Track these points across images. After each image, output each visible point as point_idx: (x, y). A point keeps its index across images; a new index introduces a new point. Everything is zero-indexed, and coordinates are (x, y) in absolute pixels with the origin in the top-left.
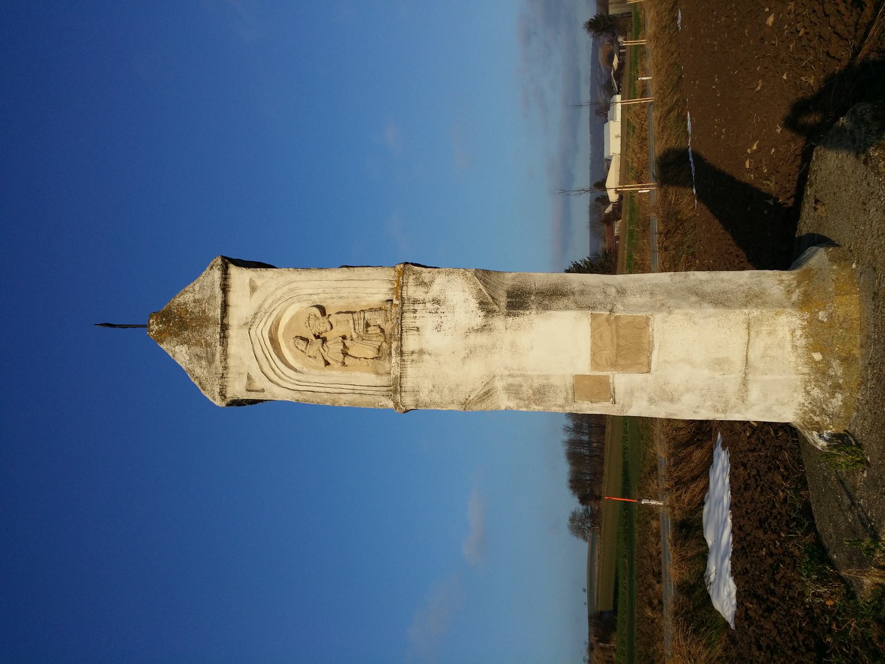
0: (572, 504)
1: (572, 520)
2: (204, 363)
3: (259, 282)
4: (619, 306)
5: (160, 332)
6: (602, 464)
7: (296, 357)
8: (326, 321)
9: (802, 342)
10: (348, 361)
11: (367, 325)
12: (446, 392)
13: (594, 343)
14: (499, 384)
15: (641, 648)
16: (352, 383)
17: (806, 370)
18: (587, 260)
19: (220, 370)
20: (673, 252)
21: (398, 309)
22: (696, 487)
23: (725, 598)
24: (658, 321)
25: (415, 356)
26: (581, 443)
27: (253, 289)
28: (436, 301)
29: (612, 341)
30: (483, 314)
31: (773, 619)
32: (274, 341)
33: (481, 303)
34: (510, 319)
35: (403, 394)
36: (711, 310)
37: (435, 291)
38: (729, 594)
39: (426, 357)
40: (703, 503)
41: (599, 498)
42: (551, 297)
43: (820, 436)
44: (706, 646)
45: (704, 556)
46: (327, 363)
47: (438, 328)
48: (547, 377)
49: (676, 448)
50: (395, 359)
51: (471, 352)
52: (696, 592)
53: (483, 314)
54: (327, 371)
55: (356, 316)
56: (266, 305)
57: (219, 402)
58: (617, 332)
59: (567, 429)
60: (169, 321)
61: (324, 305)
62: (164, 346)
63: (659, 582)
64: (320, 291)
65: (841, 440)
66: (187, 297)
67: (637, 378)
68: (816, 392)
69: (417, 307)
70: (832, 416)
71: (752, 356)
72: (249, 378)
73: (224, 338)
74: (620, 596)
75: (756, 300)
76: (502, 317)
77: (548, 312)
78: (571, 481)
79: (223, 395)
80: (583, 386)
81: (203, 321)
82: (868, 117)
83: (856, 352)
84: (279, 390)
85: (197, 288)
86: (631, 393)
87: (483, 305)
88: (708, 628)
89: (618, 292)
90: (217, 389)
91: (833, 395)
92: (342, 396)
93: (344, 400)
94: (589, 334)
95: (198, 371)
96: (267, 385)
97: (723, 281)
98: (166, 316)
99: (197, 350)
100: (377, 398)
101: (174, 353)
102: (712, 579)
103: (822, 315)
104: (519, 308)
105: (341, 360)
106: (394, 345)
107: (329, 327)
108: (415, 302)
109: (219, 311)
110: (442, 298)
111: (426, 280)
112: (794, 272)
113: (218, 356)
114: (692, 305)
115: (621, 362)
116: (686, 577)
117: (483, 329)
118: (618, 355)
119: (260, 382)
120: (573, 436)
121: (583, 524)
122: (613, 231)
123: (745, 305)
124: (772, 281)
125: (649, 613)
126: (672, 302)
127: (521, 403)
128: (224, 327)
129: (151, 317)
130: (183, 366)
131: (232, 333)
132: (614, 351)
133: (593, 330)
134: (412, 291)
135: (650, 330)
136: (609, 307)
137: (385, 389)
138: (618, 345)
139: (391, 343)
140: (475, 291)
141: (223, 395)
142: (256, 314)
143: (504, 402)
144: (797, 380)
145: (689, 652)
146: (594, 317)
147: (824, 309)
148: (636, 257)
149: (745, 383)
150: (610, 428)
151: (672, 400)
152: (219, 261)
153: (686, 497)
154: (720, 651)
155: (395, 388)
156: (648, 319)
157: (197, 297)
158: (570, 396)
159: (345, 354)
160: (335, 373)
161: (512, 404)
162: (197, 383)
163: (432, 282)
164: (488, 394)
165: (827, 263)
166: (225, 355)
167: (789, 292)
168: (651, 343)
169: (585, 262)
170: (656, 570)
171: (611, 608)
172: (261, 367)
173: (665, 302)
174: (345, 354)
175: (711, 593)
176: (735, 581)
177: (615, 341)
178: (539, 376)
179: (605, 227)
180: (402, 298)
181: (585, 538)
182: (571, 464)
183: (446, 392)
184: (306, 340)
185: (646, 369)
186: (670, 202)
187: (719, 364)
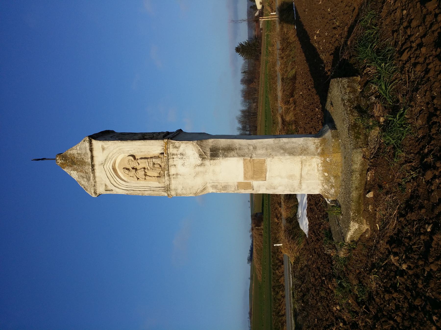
2: (85, 180)
3: (105, 146)
4: (254, 155)
5: (62, 164)
7: (124, 176)
8: (136, 162)
9: (321, 168)
10: (147, 178)
11: (154, 164)
12: (188, 189)
13: (245, 170)
14: (208, 185)
15: (273, 235)
16: (148, 186)
17: (322, 179)
18: (247, 42)
19: (93, 183)
20: (285, 60)
21: (166, 158)
23: (304, 225)
24: (269, 161)
25: (174, 176)
27: (103, 149)
28: (182, 154)
30: (201, 159)
31: (319, 244)
32: (114, 169)
33: (200, 155)
34: (212, 161)
35: (171, 191)
36: (288, 157)
37: (181, 150)
38: (306, 224)
39: (179, 176)
42: (228, 151)
43: (328, 200)
44: (297, 244)
45: (296, 206)
46: (138, 179)
47: (183, 165)
48: (227, 183)
50: (167, 178)
51: (197, 174)
52: (293, 221)
53: (201, 159)
54: (138, 181)
55: (149, 160)
56: (110, 156)
57: (94, 196)
58: (253, 165)
60: (66, 160)
61: (134, 154)
62: (65, 170)
63: (280, 207)
64: (133, 149)
65: (335, 201)
66: (74, 151)
67: (261, 182)
68: (326, 186)
69: (174, 156)
70: (331, 195)
71: (303, 174)
72: (106, 185)
73: (93, 170)
74: (264, 207)
75: (305, 152)
76: (209, 160)
77: (227, 158)
79: (95, 193)
80: (240, 185)
81: (82, 163)
82: (346, 86)
84: (119, 190)
85: (78, 148)
86: (259, 187)
87: (201, 155)
88: (298, 237)
89: (254, 148)
90: (93, 191)
91: (331, 188)
92: (145, 192)
93: (146, 193)
95: (83, 183)
96: (113, 188)
97: (293, 142)
98: (65, 158)
99: (82, 174)
100: (160, 192)
101: (71, 174)
102: (300, 216)
103: (328, 159)
104: (215, 157)
105: (144, 178)
106: (166, 172)
107: (138, 165)
108: (173, 155)
109: (90, 160)
110: (184, 153)
111: (177, 146)
112: (320, 138)
113: (92, 178)
114: (281, 154)
115: (255, 176)
116: (289, 215)
117: (201, 165)
118: (254, 174)
119: (110, 187)
120: (242, 132)
122: (259, 26)
123: (300, 154)
124: (311, 143)
125: (276, 220)
126: (273, 153)
127: (218, 191)
128: (93, 166)
129: (57, 156)
130: (75, 179)
131: (96, 167)
134: (171, 150)
136: (250, 155)
137: (163, 188)
138: (254, 170)
139: (164, 171)
140: (197, 150)
141: (95, 193)
142: (106, 160)
143: (211, 190)
144: (319, 182)
145: (290, 247)
147: (329, 157)
148: (270, 49)
149: (300, 183)
150: (260, 119)
151: (274, 189)
152: (88, 139)
154: (303, 246)
155: (167, 189)
156: (265, 160)
157: (79, 152)
158: (237, 188)
159: (146, 175)
160: (141, 182)
161: (214, 191)
162: (83, 187)
163: (179, 147)
164: (204, 189)
165: (331, 138)
166: (94, 177)
167: (317, 148)
168: (266, 169)
169: (246, 43)
170: (279, 202)
171: (261, 211)
172: (110, 181)
173: (272, 152)
174: (146, 175)
175: (299, 222)
176: (308, 219)
178: (224, 183)
179: (255, 23)
180: (168, 154)
183: (188, 189)
184: (128, 169)
185: (264, 179)
186: (284, 32)
187: (291, 177)
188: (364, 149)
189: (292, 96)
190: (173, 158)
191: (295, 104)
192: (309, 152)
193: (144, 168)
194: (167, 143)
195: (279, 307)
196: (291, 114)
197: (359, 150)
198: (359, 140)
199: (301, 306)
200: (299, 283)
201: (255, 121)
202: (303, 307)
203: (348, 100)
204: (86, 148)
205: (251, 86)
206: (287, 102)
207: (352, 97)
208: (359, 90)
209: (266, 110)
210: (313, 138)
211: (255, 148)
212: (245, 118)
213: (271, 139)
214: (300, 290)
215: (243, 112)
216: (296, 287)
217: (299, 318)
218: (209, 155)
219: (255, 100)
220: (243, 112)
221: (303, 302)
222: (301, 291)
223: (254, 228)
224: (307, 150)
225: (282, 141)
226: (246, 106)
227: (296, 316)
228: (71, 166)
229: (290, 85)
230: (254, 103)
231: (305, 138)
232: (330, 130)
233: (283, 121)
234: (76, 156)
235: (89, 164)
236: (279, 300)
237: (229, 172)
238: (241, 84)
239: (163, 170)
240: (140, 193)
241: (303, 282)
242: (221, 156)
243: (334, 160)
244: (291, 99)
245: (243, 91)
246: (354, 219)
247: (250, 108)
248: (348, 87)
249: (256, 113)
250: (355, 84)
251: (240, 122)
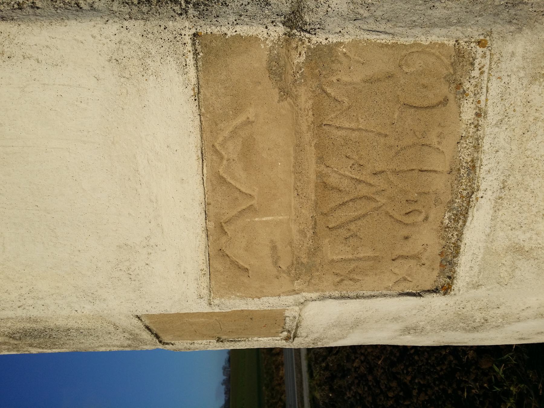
13: (217, 183)
29: (298, 169)
58: (319, 126)
94: (193, 141)
115: (334, 250)
132: (307, 213)
135: (468, 112)
138: (324, 186)
146: (208, 53)
156: (461, 58)
177: (312, 167)
185: (429, 277)
199: (328, 396)
214: (324, 364)
221: (331, 390)
222: (327, 368)
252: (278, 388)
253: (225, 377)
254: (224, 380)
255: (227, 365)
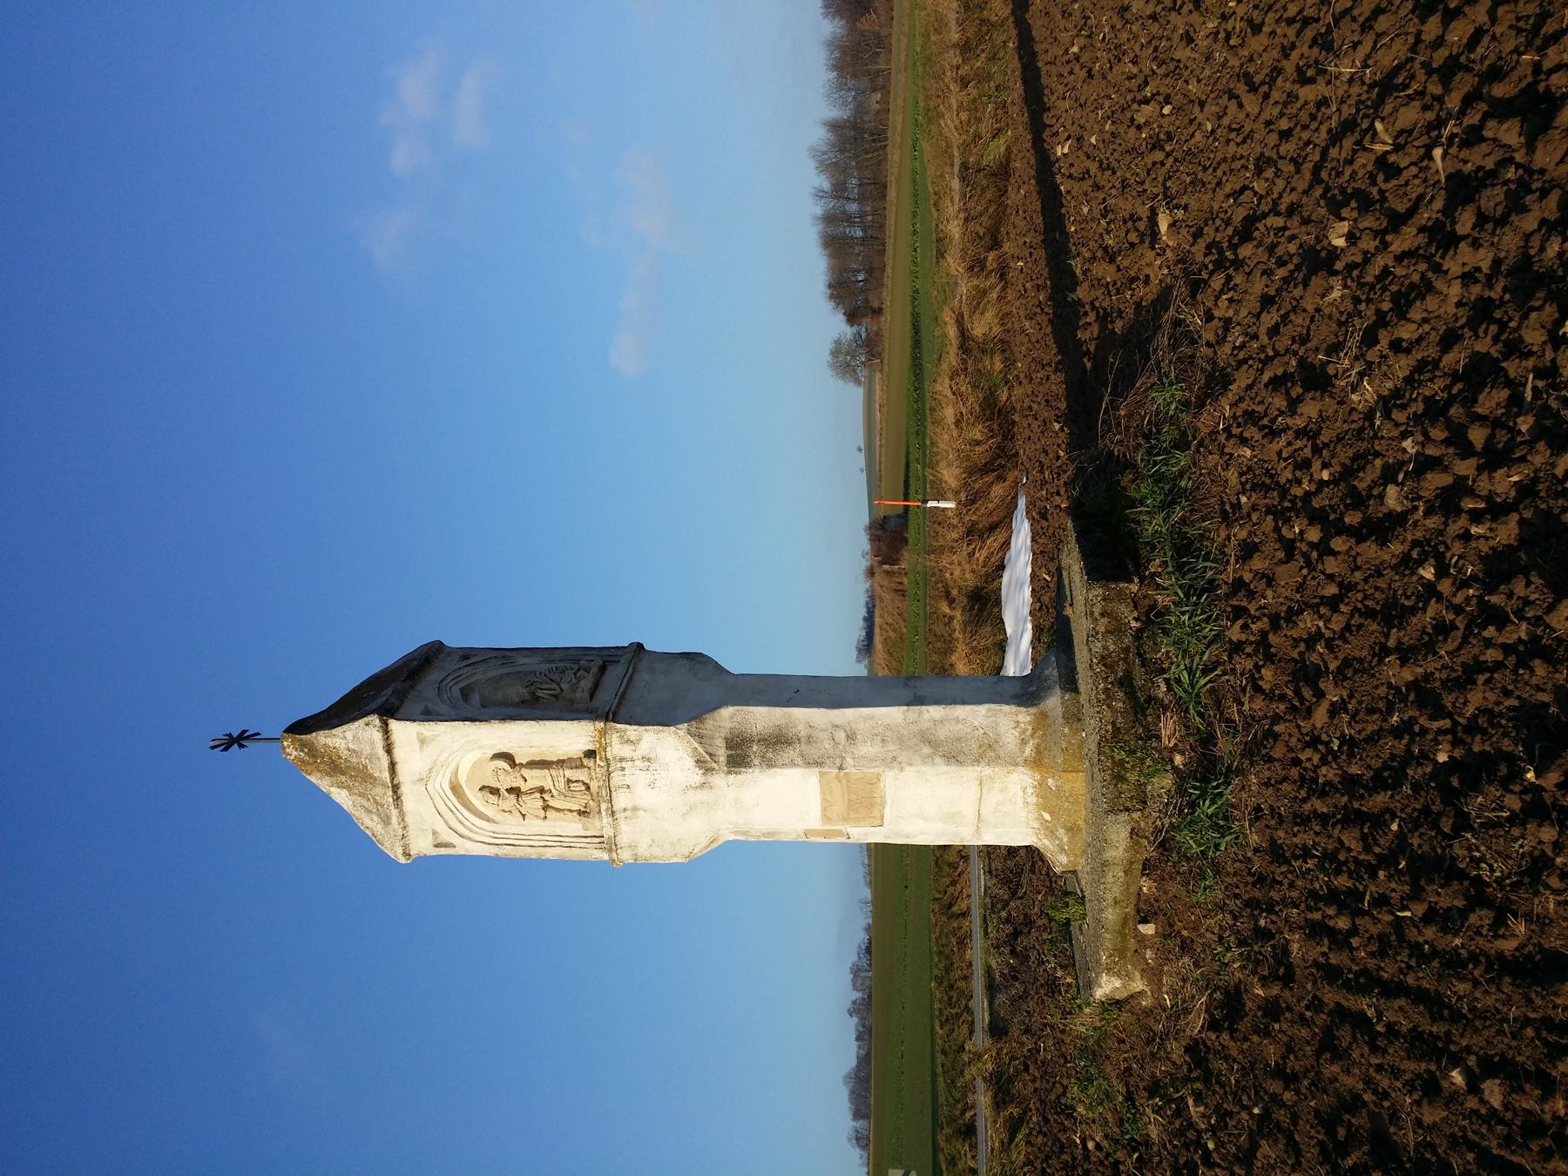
0: (835, 326)
1: (835, 353)
4: (849, 760)
6: (882, 253)
10: (550, 814)
12: (667, 846)
13: (824, 799)
20: (974, 93)
21: (603, 771)
22: (993, 542)
25: (628, 813)
26: (848, 219)
27: (423, 741)
32: (456, 788)
34: (732, 777)
39: (641, 813)
40: (1002, 567)
41: (878, 312)
47: (652, 785)
49: (970, 475)
50: (606, 820)
51: (691, 809)
56: (442, 759)
57: (402, 860)
59: (820, 194)
62: (313, 779)
71: (983, 812)
72: (434, 833)
73: (397, 798)
78: (830, 286)
79: (407, 854)
82: (1097, 611)
83: (1081, 823)
90: (400, 851)
95: (367, 822)
97: (958, 721)
99: (364, 802)
106: (604, 806)
108: (622, 760)
110: (653, 756)
112: (1033, 710)
113: (394, 820)
115: (853, 815)
121: (853, 357)
126: (902, 757)
128: (396, 788)
131: (405, 790)
133: (822, 786)
134: (616, 749)
141: (407, 854)
150: (896, 157)
153: (981, 555)
155: (611, 845)
166: (402, 815)
167: (1024, 742)
174: (546, 808)
181: (858, 382)
182: (830, 256)
183: (667, 846)
188: (1136, 815)
189: (996, 244)
190: (623, 769)
191: (1002, 276)
192: (1002, 754)
193: (542, 790)
194: (603, 733)
195: (951, 889)
196: (989, 315)
197: (1124, 817)
198: (1125, 787)
200: (1003, 893)
201: (879, 163)
202: (1012, 968)
203: (1103, 657)
204: (372, 743)
205: (864, 25)
206: (976, 266)
207: (1112, 647)
208: (1134, 624)
209: (915, 172)
210: (1014, 708)
211: (851, 737)
212: (842, 151)
213: (896, 709)
214: (1004, 914)
215: (834, 126)
216: (993, 905)
217: (1001, 998)
218: (722, 759)
219: (879, 82)
220: (834, 126)
221: (1013, 953)
222: (1008, 920)
223: (877, 570)
224: (996, 746)
225: (926, 716)
226: (845, 104)
227: (992, 989)
228: (328, 774)
229: (989, 195)
230: (874, 90)
231: (992, 706)
232: (1058, 691)
233: (964, 335)
234: (345, 754)
235: (384, 785)
236: (954, 866)
237: (782, 802)
238: (825, 15)
239: (597, 798)
240: (533, 853)
241: (1014, 894)
242: (756, 762)
243: (1067, 787)
244: (991, 256)
245: (831, 44)
246: (1109, 969)
247: (860, 110)
248: (1102, 615)
249: (885, 132)
250: (1123, 608)
251: (825, 167)
252: (961, 984)
253: (857, 995)
254: (854, 1002)
255: (864, 963)
